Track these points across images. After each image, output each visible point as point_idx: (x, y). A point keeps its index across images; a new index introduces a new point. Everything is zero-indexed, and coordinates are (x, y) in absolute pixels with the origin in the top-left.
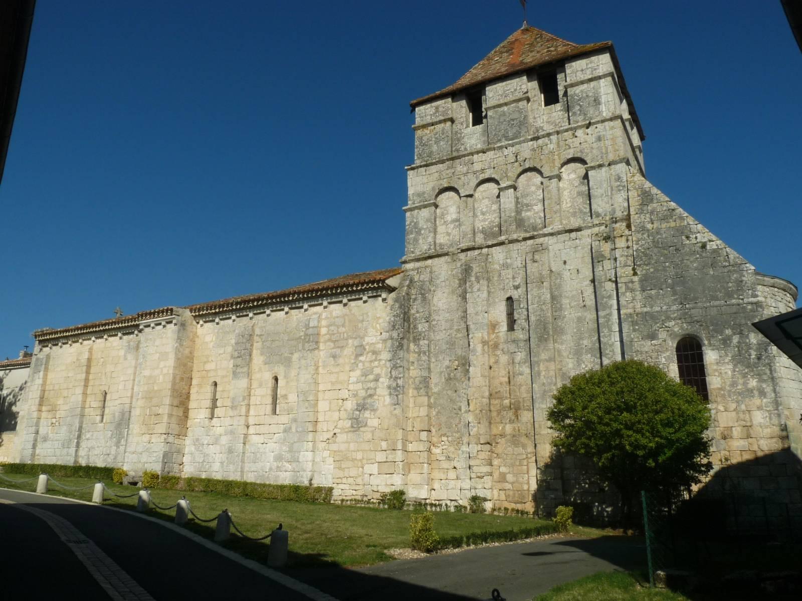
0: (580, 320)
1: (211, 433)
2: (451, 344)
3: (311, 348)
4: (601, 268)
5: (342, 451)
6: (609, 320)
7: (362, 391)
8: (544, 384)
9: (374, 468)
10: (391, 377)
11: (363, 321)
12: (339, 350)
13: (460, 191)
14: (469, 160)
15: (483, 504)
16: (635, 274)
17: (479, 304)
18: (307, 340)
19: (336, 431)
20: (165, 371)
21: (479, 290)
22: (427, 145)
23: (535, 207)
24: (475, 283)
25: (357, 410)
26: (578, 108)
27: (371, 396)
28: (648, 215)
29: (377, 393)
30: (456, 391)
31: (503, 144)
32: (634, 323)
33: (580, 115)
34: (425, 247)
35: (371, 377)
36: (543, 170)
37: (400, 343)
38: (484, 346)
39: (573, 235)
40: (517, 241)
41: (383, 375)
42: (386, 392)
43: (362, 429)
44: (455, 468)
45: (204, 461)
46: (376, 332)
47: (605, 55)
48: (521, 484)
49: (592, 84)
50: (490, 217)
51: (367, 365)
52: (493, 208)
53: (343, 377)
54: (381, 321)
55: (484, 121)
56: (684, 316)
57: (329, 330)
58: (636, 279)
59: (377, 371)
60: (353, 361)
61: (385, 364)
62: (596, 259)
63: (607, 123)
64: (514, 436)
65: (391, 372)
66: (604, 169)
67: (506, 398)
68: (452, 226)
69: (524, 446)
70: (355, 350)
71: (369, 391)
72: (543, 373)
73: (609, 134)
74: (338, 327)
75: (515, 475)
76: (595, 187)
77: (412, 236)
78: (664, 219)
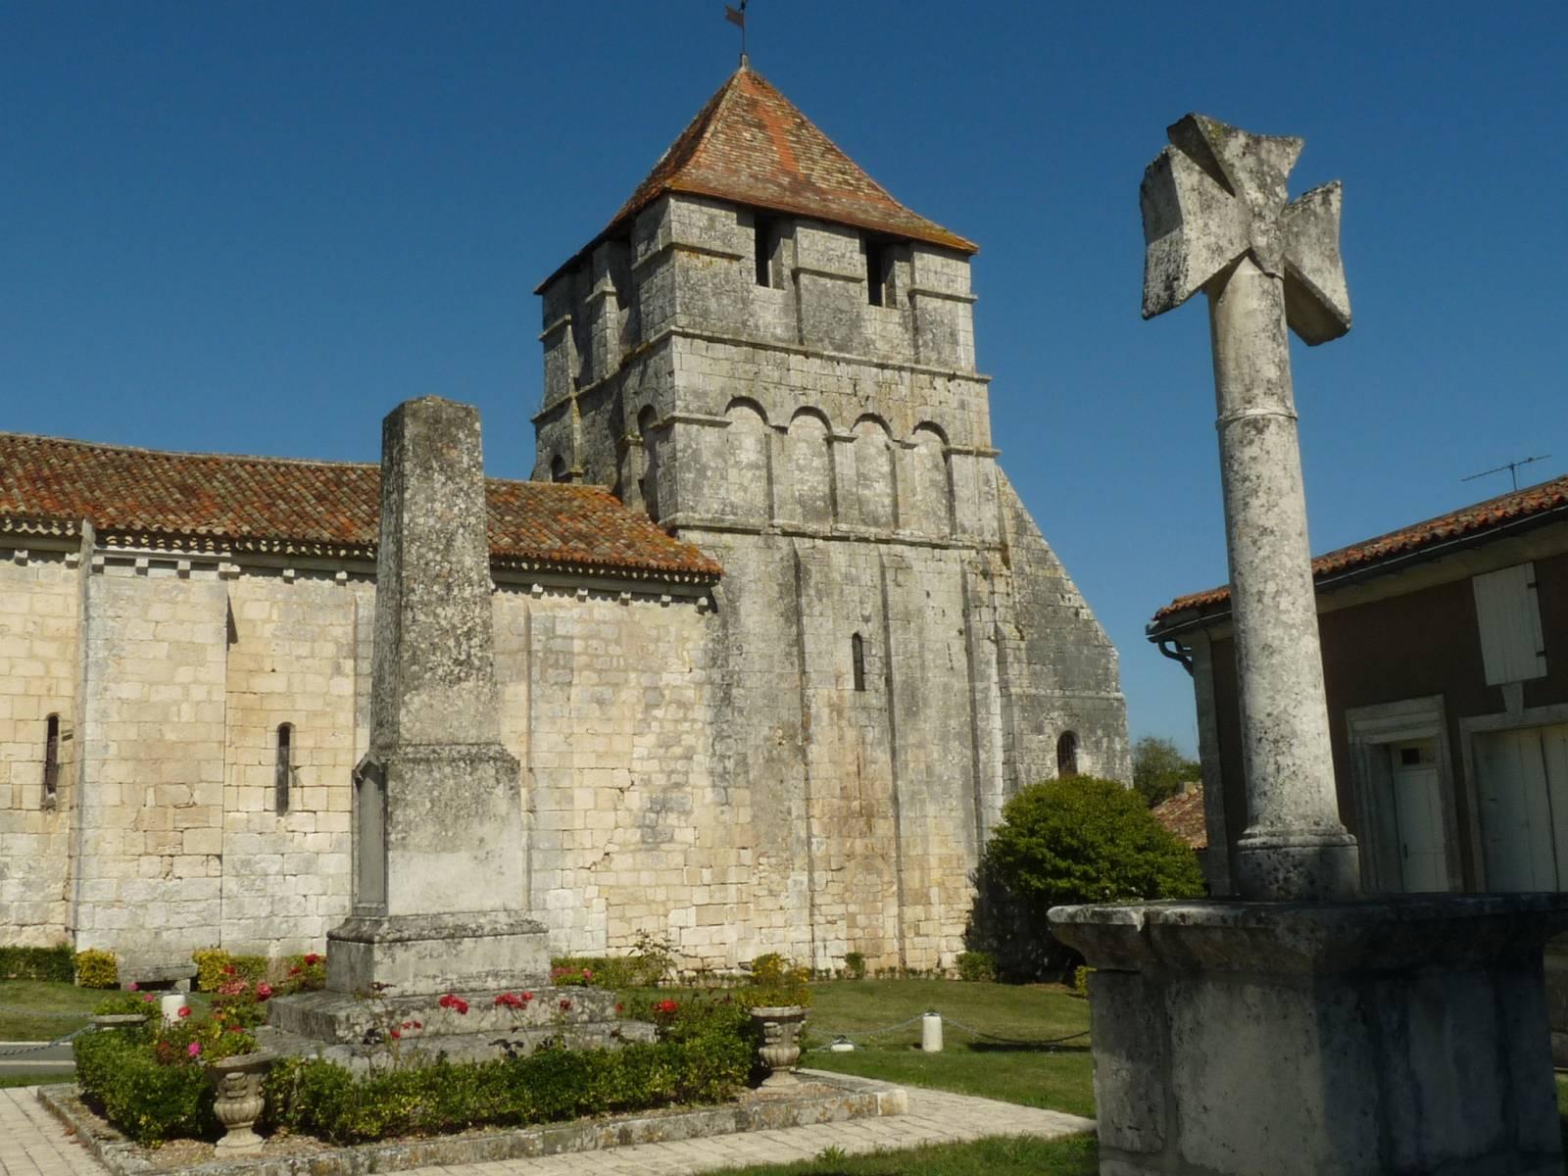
0: (946, 688)
1: (289, 848)
2: (772, 699)
3: (560, 680)
4: (978, 618)
5: (625, 888)
6: (987, 697)
7: (660, 776)
8: (912, 782)
9: (690, 917)
10: (714, 754)
11: (658, 640)
12: (610, 690)
13: (768, 414)
15: (82, 958)
16: (1022, 638)
17: (822, 638)
18: (551, 662)
19: (610, 848)
20: (198, 693)
21: (821, 615)
22: (698, 292)
23: (876, 485)
24: (816, 602)
25: (651, 810)
27: (677, 785)
29: (691, 781)
30: (782, 781)
32: (1023, 709)
34: (716, 506)
35: (678, 751)
36: (893, 426)
37: (726, 694)
38: (832, 711)
39: (937, 551)
40: (866, 540)
41: (700, 749)
42: (706, 781)
43: (663, 846)
44: (781, 908)
45: (272, 914)
46: (684, 664)
48: (875, 928)
49: (949, 304)
50: (810, 478)
51: (669, 726)
52: (814, 464)
53: (620, 744)
54: (689, 645)
56: (1066, 707)
57: (587, 647)
58: (1023, 645)
59: (688, 740)
60: (639, 716)
61: (703, 728)
62: (970, 605)
64: (866, 858)
65: (713, 745)
67: (855, 799)
68: (750, 474)
69: (879, 874)
70: (644, 693)
71: (673, 776)
72: (911, 765)
73: (973, 401)
74: (607, 642)
75: (868, 916)
76: (960, 483)
77: (690, 476)
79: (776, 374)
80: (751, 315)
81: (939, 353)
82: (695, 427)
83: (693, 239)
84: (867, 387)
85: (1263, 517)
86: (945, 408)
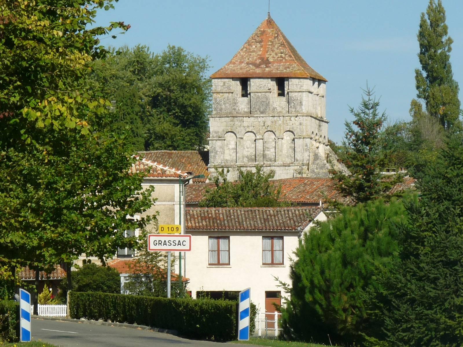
14: (242, 120)
22: (219, 104)
23: (271, 150)
26: (293, 104)
28: (316, 166)
31: (258, 115)
33: (293, 108)
34: (219, 161)
39: (287, 168)
47: (225, 240)
55: (249, 96)
63: (304, 117)
66: (301, 140)
77: (212, 154)
78: (321, 168)
79: (240, 124)
80: (237, 107)
81: (296, 109)
82: (215, 141)
83: (219, 90)
84: (268, 123)
85: (102, 146)
86: (294, 126)
